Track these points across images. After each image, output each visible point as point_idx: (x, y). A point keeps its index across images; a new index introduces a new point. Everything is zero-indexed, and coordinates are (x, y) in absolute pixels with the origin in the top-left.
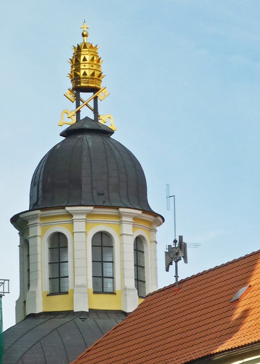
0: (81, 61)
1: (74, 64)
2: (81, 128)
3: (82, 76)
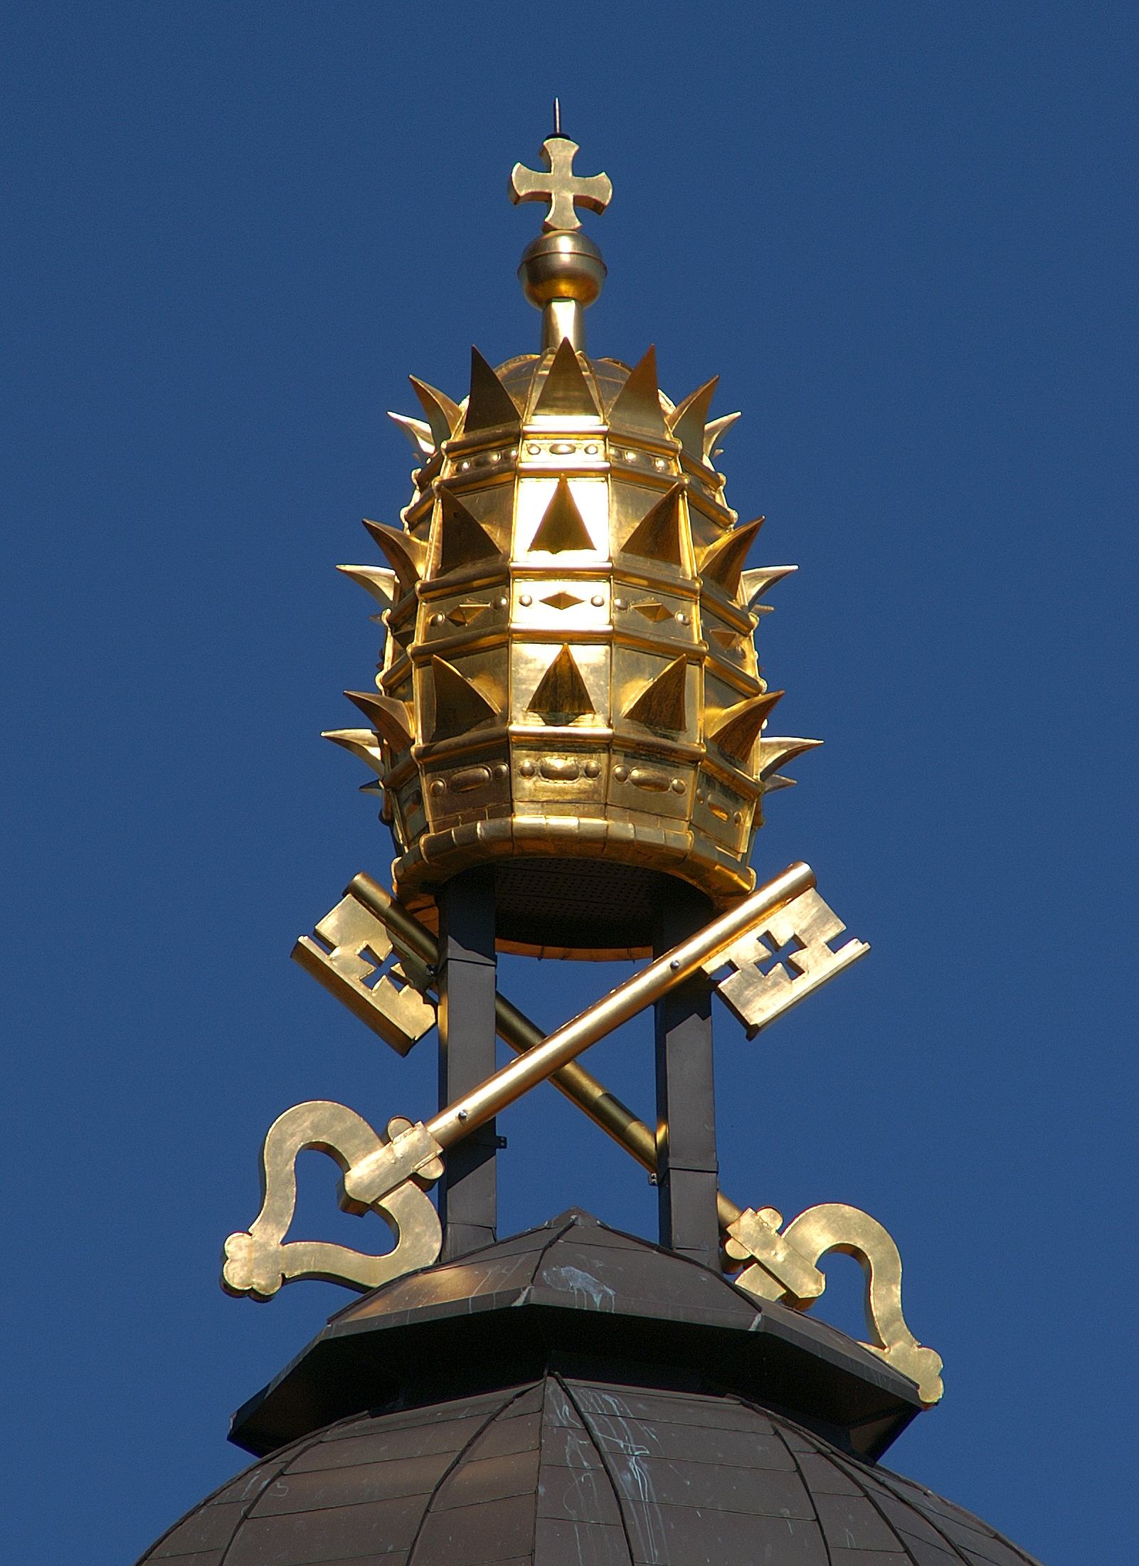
0: (521, 552)
1: (418, 652)
2: (519, 1302)
3: (527, 723)
